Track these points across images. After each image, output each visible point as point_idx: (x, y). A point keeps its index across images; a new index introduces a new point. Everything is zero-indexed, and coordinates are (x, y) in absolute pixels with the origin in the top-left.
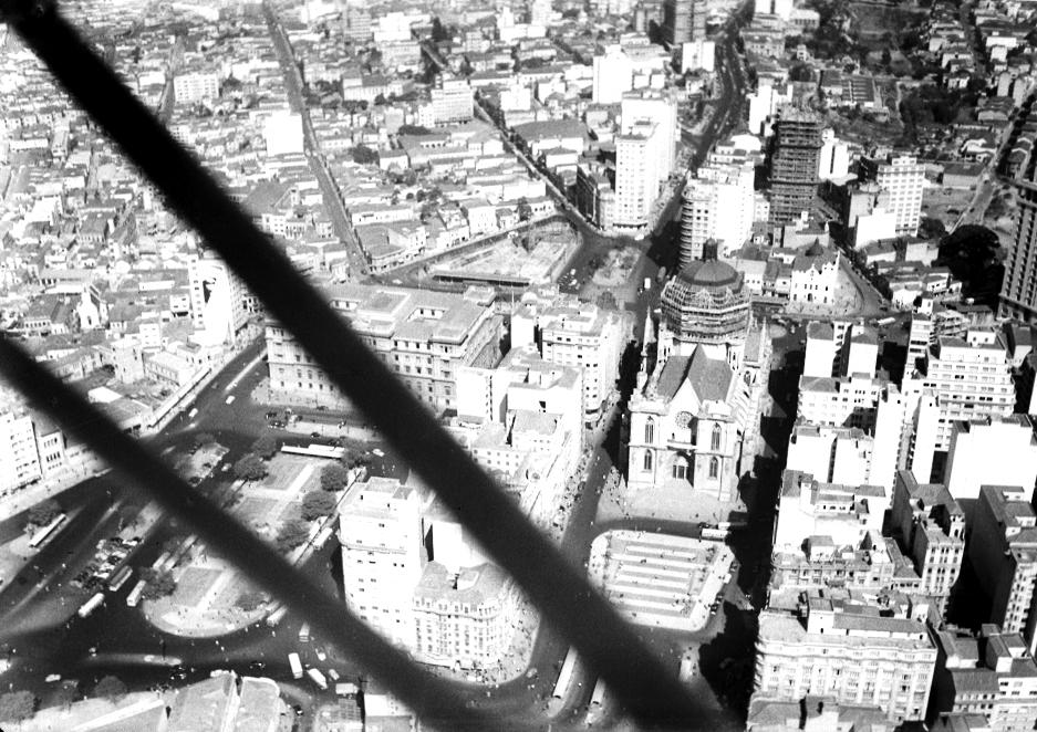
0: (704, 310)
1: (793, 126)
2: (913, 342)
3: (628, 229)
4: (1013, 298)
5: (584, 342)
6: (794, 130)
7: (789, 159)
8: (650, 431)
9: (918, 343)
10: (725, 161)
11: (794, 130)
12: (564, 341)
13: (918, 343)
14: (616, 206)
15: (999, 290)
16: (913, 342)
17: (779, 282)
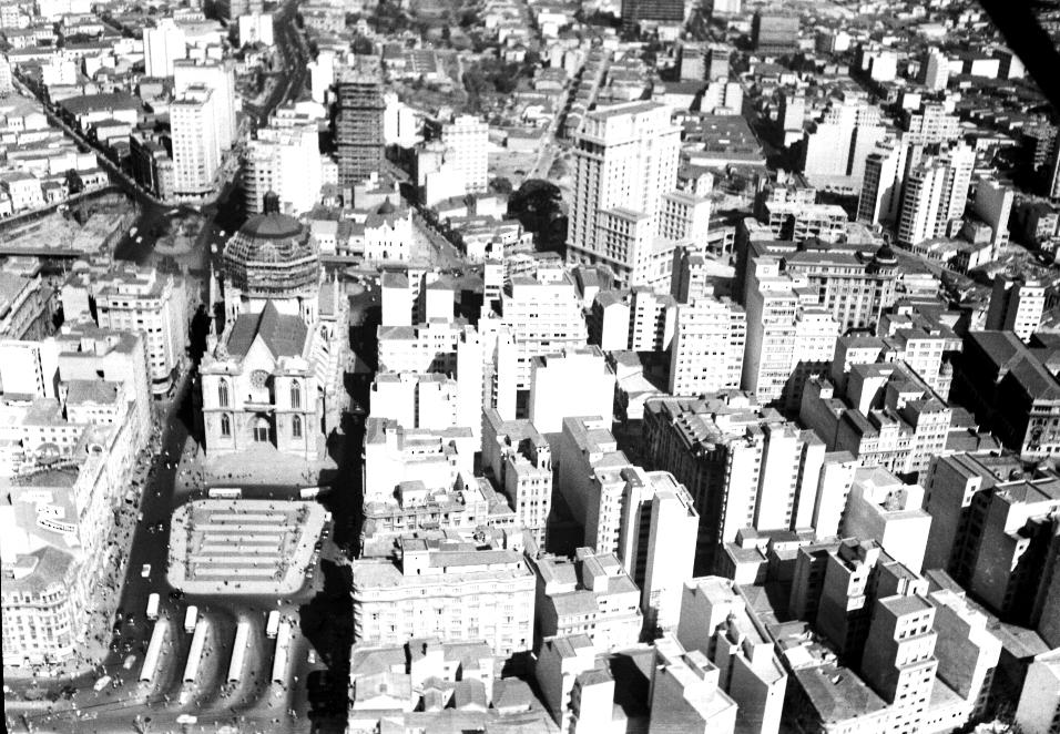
1: (354, 88)
10: (287, 125)
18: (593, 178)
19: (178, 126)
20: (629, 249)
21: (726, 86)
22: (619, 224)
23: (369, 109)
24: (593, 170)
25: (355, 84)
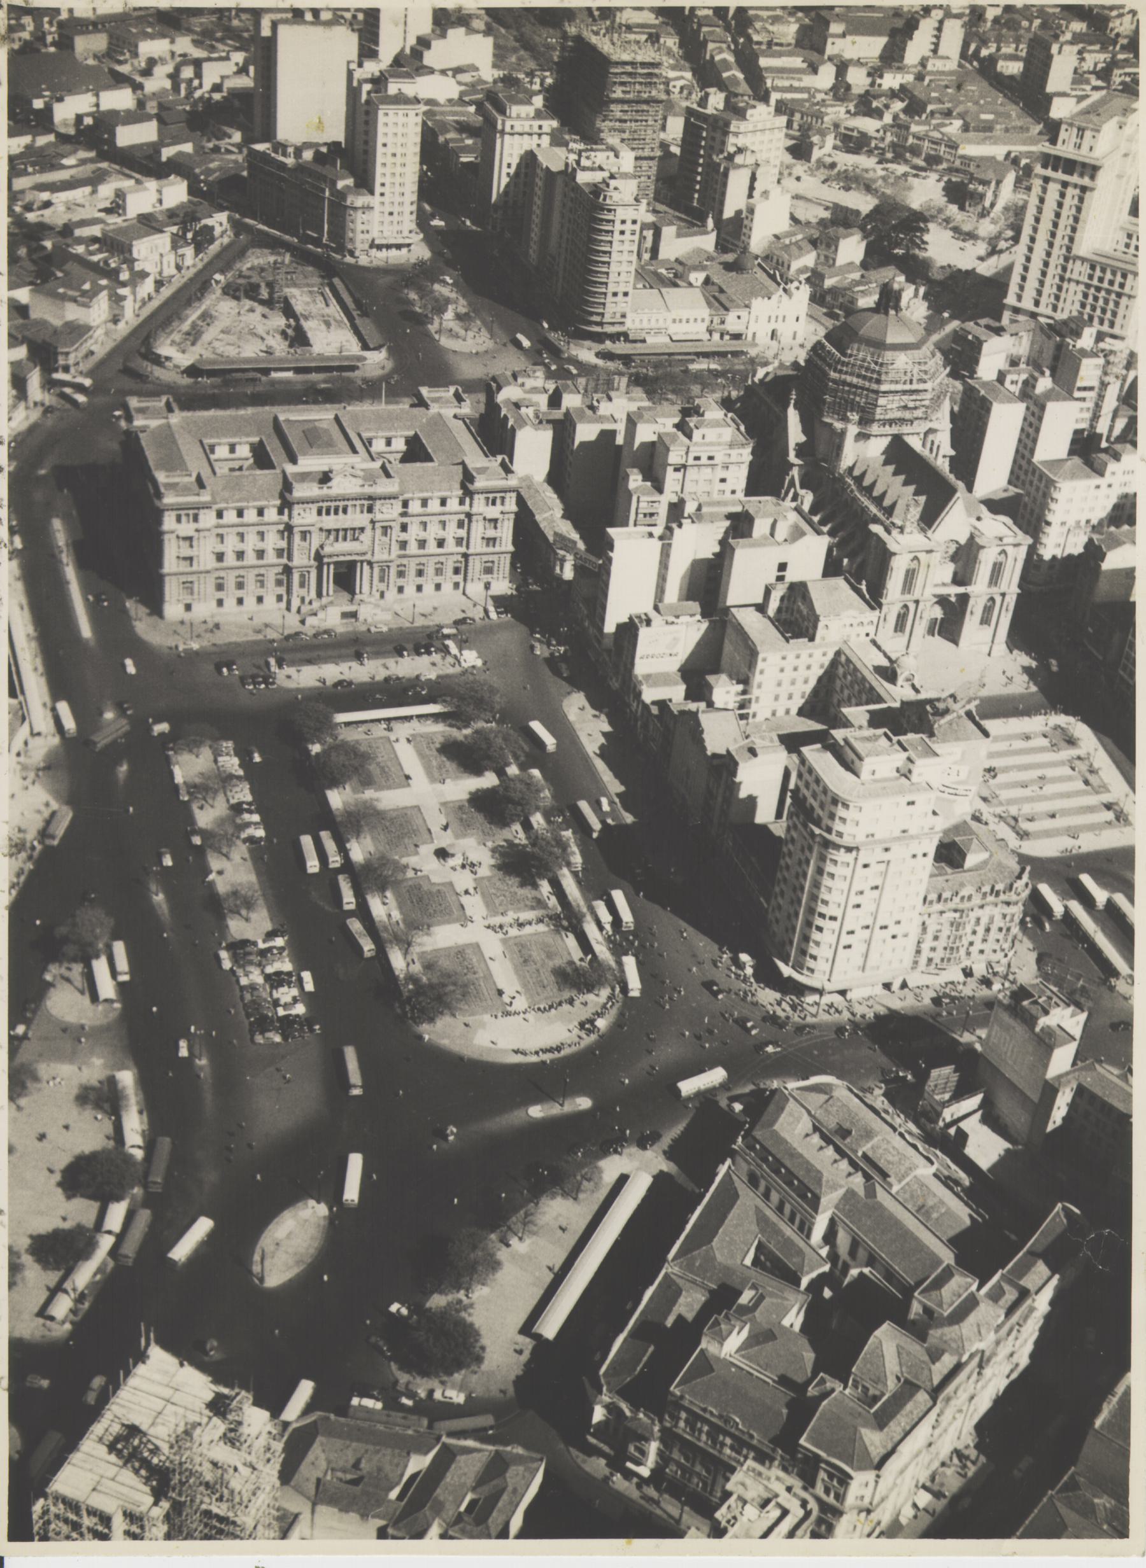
0: (907, 387)
1: (629, 69)
2: (1080, 389)
3: (393, 252)
4: (1027, 304)
5: (733, 459)
6: (630, 74)
7: (621, 121)
8: (910, 576)
9: (1085, 389)
10: (527, 129)
11: (630, 74)
12: (704, 460)
13: (1085, 389)
14: (375, 216)
15: (1005, 295)
16: (1080, 389)
17: (731, 317)
18: (1067, 212)
19: (389, 140)
20: (1121, 311)
21: (941, 22)
22: (1108, 276)
23: (647, 102)
24: (1070, 201)
25: (632, 64)
